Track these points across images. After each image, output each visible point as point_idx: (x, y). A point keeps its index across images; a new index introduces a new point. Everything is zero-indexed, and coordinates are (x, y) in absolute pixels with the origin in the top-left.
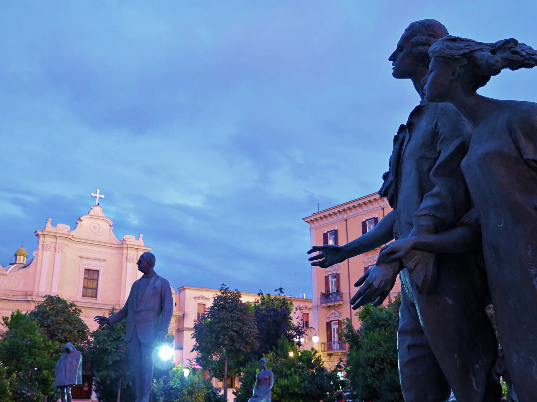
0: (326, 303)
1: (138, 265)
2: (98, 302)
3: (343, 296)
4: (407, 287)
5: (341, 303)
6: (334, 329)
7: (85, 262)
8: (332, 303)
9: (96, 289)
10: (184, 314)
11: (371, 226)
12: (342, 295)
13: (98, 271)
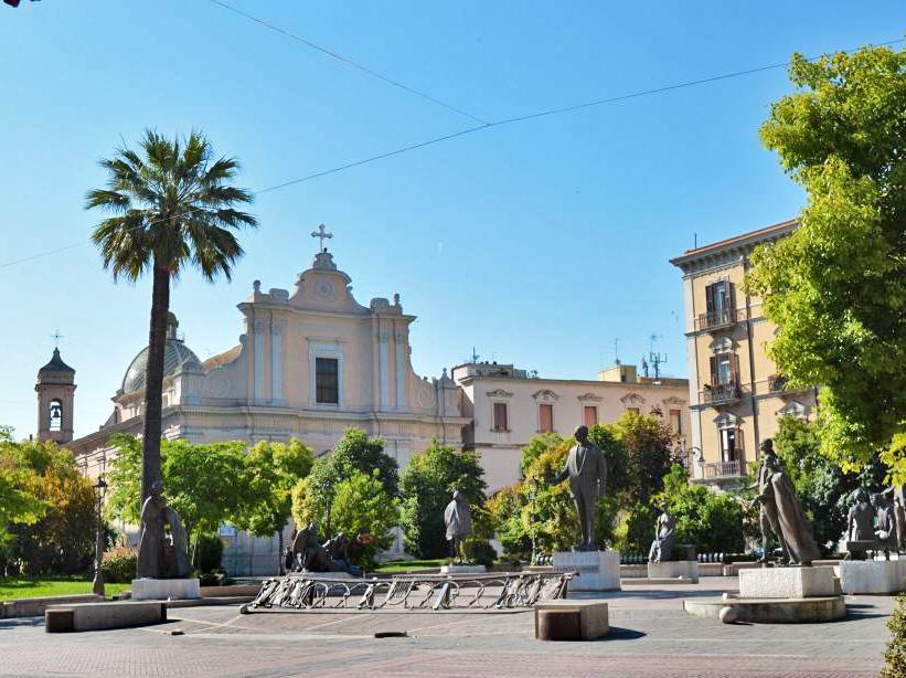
4: (790, 234)
10: (473, 423)
13: (336, 361)
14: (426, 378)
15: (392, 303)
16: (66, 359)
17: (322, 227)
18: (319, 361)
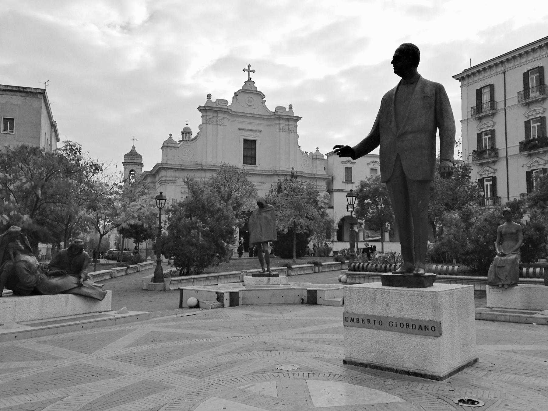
0: (479, 160)
1: (393, 65)
2: (258, 169)
3: (498, 152)
5: (496, 159)
6: (487, 186)
7: (244, 133)
8: (486, 159)
9: (255, 157)
11: (534, 76)
12: (496, 151)
14: (306, 153)
15: (288, 109)
16: (138, 151)
17: (249, 66)
18: (246, 141)
